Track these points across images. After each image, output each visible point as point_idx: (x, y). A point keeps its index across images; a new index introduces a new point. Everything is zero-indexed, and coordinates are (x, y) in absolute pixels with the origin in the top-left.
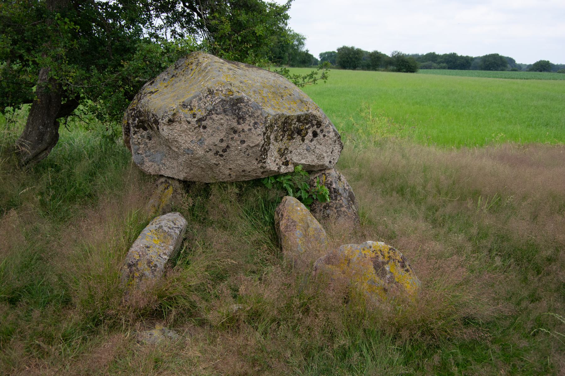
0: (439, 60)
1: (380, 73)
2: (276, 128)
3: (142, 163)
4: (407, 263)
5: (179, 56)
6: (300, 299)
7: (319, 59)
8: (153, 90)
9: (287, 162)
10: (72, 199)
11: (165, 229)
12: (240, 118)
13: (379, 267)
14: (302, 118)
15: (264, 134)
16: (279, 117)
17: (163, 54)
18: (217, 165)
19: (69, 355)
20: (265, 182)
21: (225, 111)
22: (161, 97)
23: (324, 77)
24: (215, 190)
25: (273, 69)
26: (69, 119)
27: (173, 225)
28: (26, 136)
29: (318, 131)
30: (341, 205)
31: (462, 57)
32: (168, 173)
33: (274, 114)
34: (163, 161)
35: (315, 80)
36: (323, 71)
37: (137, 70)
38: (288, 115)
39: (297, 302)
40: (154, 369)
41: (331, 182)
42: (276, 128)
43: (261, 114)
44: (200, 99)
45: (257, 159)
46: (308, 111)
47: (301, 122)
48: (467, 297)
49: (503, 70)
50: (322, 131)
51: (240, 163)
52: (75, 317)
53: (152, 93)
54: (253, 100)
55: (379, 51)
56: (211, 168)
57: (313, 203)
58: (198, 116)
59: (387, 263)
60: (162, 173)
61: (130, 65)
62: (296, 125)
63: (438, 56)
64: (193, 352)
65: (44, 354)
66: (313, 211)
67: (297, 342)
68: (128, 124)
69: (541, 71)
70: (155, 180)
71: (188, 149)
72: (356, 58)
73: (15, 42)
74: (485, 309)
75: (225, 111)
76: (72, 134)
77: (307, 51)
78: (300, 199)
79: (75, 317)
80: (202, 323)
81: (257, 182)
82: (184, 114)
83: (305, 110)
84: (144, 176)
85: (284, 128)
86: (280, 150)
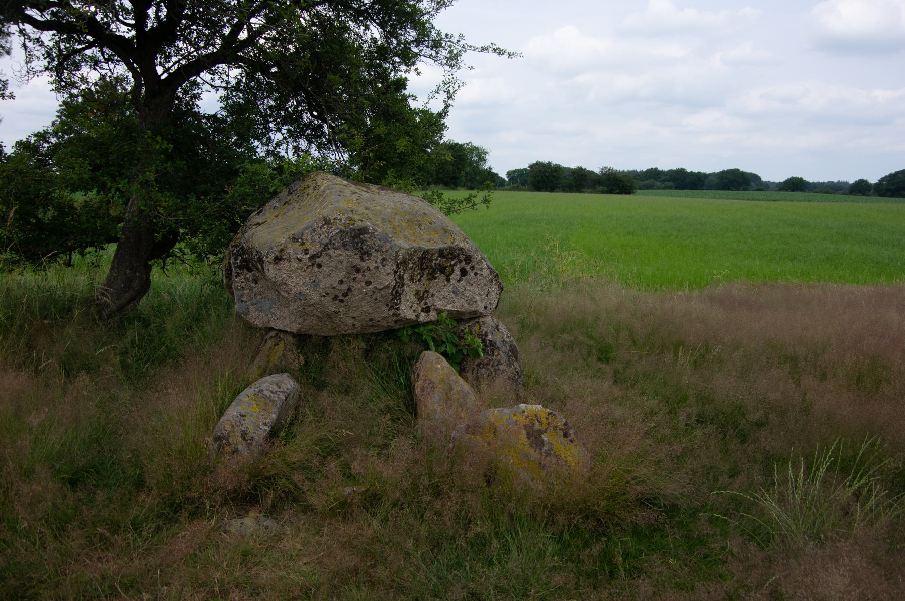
0: (663, 178)
1: (586, 195)
2: (411, 265)
3: (247, 313)
4: (571, 432)
5: (291, 177)
6: (430, 477)
7: (507, 179)
8: (260, 221)
9: (429, 308)
10: (162, 361)
11: (267, 393)
12: (364, 253)
13: (535, 437)
14: (446, 252)
15: (395, 272)
16: (415, 251)
17: (272, 177)
18: (337, 313)
19: (139, 547)
20: (399, 334)
21: (344, 245)
22: (267, 231)
23: (486, 201)
24: (335, 345)
25: (421, 194)
26: (169, 261)
27: (276, 388)
28: (109, 283)
29: (468, 268)
30: (499, 361)
31: (692, 174)
32: (279, 325)
33: (408, 247)
34: (273, 310)
35: (474, 205)
36: (485, 193)
37: (244, 197)
38: (426, 248)
39: (425, 480)
40: (241, 564)
41: (486, 332)
42: (411, 265)
43: (391, 248)
44: (314, 231)
45: (387, 305)
46: (453, 243)
47: (444, 257)
48: (642, 471)
49: (745, 190)
50: (473, 268)
51: (364, 310)
52: (148, 501)
53: (259, 224)
54: (380, 230)
55: (583, 167)
56: (330, 317)
57: (463, 360)
58: (312, 251)
59: (545, 431)
60: (272, 325)
61: (236, 191)
62: (437, 260)
63: (662, 172)
64: (291, 544)
65: (107, 544)
66: (461, 372)
67: (424, 531)
68: (229, 263)
69: (793, 191)
70: (263, 336)
71: (300, 293)
72: (554, 177)
73: (95, 168)
74: (672, 487)
75: (344, 245)
76: (174, 281)
77: (490, 169)
78: (445, 355)
79: (148, 501)
80: (307, 509)
81: (390, 334)
82: (293, 250)
83: (449, 242)
84: (250, 328)
85: (422, 264)
86: (417, 293)
